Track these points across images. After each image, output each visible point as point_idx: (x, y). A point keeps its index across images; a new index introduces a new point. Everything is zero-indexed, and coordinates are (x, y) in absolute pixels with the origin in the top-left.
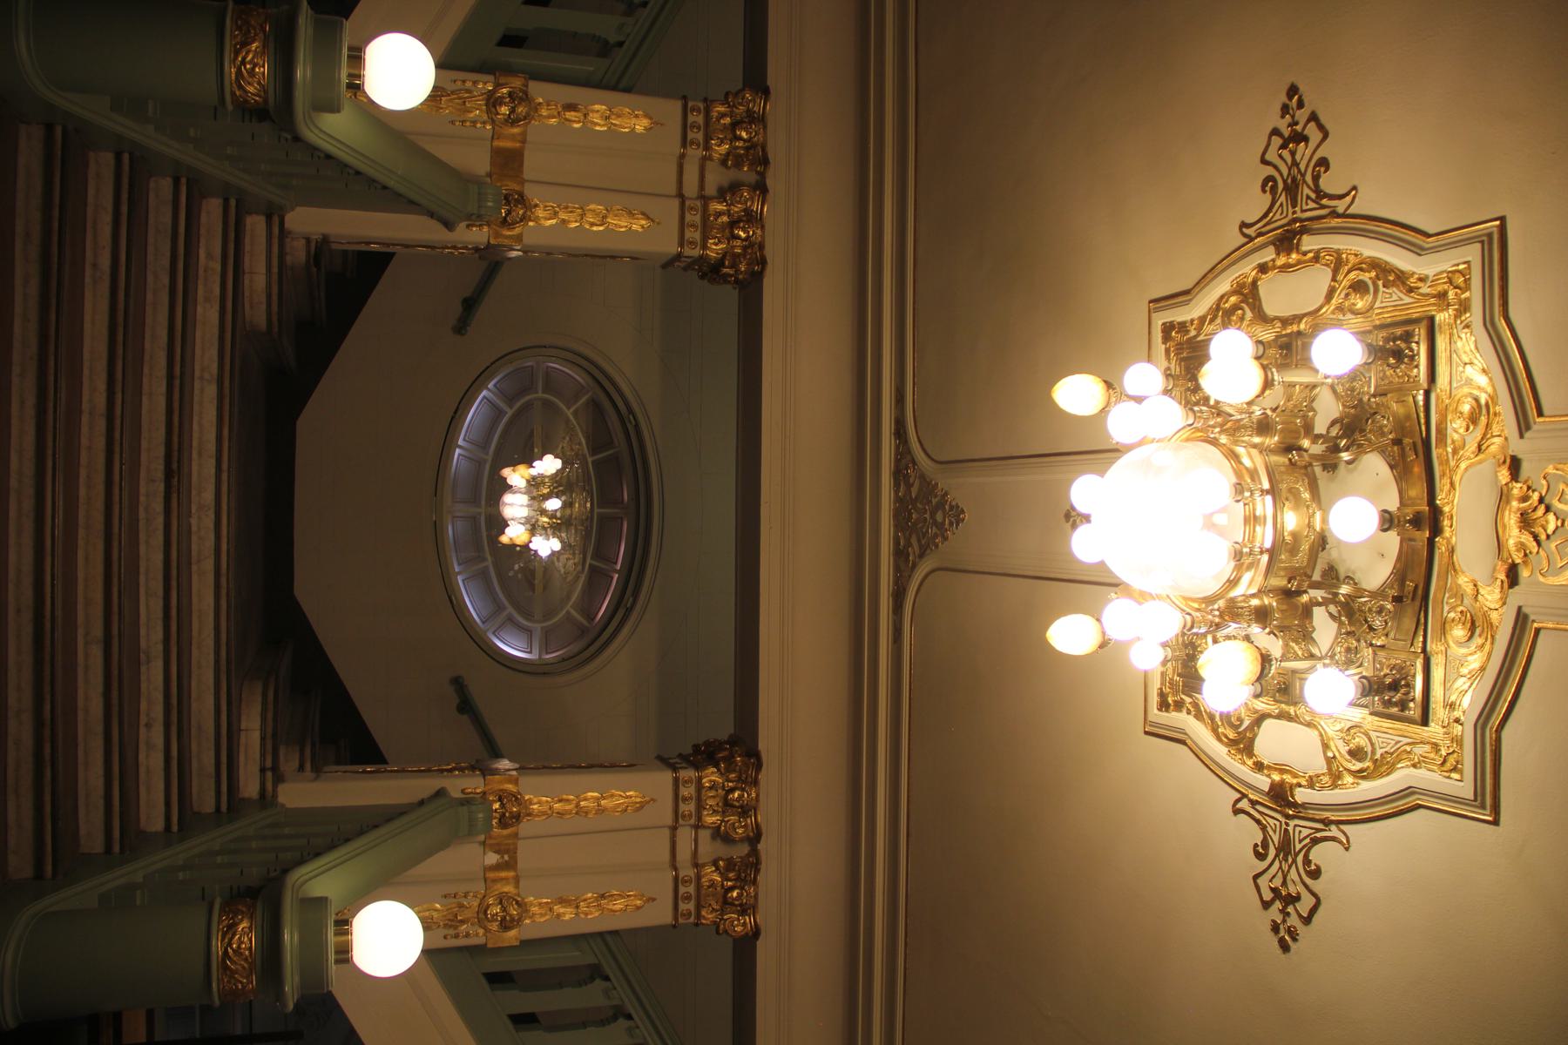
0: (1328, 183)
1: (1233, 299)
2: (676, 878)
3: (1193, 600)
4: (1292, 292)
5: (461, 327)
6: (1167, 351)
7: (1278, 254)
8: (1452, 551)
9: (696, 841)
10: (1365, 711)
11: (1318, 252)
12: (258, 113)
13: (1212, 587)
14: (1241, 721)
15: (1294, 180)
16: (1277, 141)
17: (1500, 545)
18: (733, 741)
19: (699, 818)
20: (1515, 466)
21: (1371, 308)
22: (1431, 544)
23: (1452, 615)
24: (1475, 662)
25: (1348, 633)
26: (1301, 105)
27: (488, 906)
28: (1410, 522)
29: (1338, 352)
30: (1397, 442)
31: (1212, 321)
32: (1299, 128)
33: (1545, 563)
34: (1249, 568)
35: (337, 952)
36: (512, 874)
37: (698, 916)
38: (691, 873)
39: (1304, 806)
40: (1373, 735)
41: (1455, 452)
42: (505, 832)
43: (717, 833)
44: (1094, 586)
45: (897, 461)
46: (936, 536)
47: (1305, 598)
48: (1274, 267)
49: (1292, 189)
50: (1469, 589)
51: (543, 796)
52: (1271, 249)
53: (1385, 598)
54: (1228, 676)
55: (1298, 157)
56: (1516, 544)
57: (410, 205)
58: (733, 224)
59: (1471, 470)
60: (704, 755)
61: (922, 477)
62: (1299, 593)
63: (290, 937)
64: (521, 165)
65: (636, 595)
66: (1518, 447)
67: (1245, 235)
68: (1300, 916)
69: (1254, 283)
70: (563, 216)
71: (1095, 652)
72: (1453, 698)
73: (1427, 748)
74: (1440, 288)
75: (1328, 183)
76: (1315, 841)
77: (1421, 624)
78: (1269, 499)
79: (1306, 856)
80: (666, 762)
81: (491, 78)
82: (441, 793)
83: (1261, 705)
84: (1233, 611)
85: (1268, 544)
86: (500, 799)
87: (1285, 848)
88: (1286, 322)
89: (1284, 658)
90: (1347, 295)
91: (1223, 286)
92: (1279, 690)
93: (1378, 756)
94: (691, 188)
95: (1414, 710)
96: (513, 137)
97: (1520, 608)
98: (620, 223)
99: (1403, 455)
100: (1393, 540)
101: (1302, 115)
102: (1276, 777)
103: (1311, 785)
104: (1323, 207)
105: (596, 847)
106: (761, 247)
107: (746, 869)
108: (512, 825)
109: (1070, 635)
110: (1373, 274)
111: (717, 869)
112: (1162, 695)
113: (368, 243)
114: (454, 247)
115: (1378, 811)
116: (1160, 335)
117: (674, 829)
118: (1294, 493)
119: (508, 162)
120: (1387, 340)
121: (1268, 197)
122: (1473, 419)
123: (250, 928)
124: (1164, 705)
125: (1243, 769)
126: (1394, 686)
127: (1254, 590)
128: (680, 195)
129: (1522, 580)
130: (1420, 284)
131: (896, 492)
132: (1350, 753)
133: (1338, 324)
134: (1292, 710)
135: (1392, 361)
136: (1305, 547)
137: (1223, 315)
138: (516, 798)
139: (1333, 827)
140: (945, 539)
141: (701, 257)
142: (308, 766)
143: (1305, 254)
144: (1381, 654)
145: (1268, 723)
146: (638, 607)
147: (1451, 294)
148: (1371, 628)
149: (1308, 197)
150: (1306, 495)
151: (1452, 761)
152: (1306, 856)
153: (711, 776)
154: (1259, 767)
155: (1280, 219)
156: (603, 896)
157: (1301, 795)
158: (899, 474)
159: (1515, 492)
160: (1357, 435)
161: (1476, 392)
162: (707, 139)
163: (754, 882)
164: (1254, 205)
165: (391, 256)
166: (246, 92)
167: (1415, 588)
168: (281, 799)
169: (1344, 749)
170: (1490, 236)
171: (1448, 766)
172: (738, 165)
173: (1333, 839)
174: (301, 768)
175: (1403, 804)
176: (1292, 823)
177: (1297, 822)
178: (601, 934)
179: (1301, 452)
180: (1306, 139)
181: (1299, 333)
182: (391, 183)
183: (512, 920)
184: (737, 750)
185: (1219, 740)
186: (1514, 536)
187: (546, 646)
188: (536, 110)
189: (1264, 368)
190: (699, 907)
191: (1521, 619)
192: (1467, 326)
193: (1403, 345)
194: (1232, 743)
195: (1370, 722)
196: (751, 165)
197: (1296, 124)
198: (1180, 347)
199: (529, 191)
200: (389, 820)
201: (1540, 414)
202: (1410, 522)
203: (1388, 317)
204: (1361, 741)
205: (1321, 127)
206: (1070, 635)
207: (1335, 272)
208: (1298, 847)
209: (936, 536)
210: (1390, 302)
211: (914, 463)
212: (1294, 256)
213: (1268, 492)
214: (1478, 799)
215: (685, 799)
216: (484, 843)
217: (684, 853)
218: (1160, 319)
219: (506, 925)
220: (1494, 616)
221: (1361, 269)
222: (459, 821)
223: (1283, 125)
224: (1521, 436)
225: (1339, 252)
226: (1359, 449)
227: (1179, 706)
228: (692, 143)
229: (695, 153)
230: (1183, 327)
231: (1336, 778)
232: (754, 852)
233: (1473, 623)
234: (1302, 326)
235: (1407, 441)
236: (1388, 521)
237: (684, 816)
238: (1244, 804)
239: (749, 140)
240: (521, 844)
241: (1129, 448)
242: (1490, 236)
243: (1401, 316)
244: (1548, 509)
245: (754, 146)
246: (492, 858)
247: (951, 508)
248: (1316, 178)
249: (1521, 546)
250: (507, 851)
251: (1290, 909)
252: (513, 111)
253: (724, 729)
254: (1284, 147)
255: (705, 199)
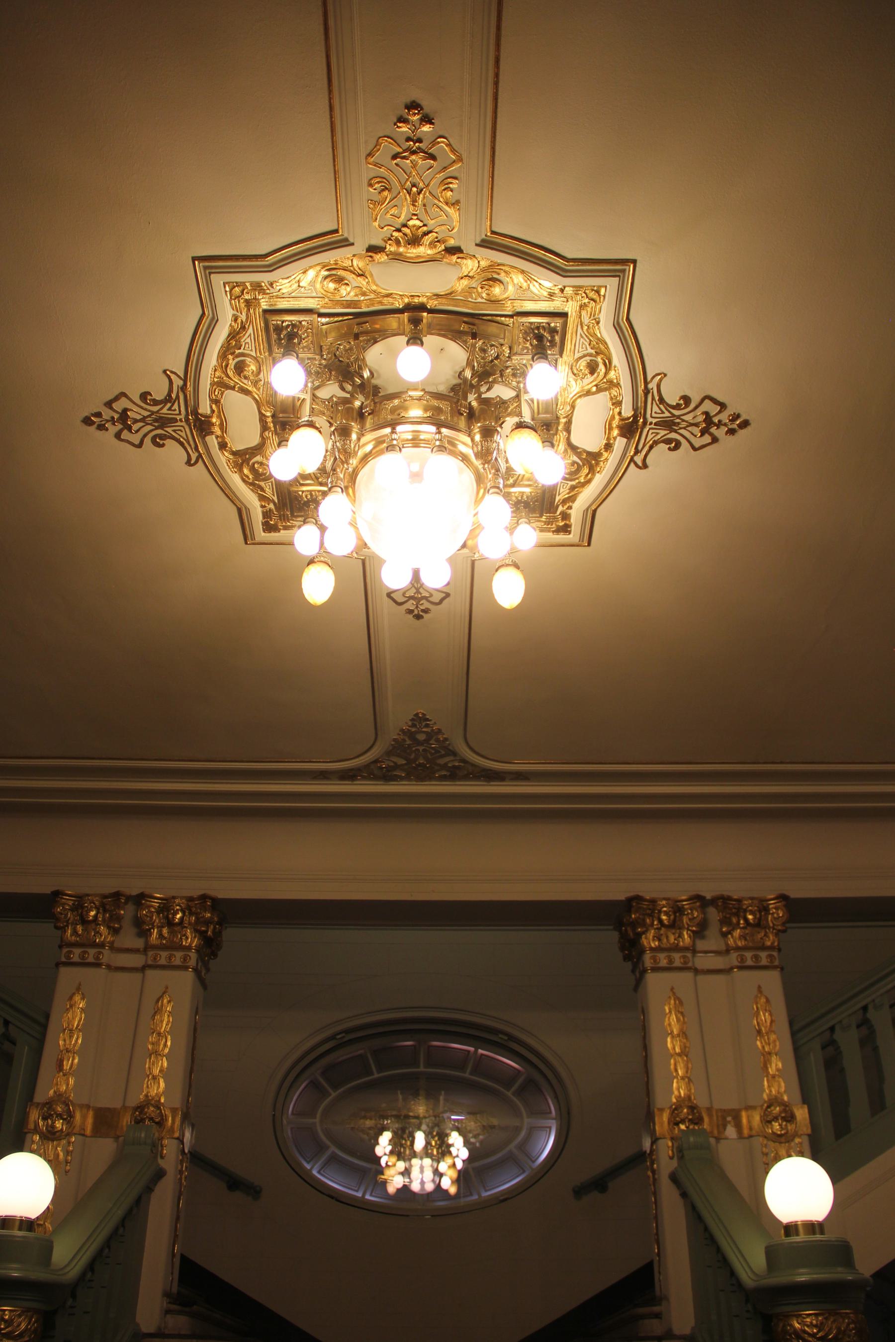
0: (159, 393)
1: (246, 471)
2: (741, 968)
3: (478, 493)
4: (242, 422)
5: (254, 1191)
6: (286, 528)
7: (212, 433)
8: (437, 296)
9: (706, 952)
10: (560, 360)
11: (211, 400)
12: (47, 1321)
13: (469, 477)
14: (574, 463)
15: (156, 420)
16: (125, 435)
17: (432, 260)
18: (619, 925)
19: (686, 949)
20: (373, 249)
21: (256, 359)
22: (431, 311)
23: (484, 295)
24: (519, 279)
25: (502, 376)
26: (98, 415)
27: (774, 1133)
28: (416, 326)
29: (288, 377)
30: (356, 337)
31: (262, 490)
32: (116, 416)
33: (443, 228)
34: (454, 445)
35: (814, 1233)
36: (744, 1114)
37: (771, 948)
38: (734, 955)
39: (635, 409)
40: (577, 355)
41: (364, 294)
42: (706, 1119)
43: (700, 932)
44: (472, 572)
45: (376, 778)
46: (437, 740)
47: (474, 404)
48: (223, 437)
49: (163, 422)
50: (465, 282)
51: (675, 1087)
52: (208, 438)
53: (474, 346)
54: (537, 461)
55: (139, 417)
56: (431, 248)
57: (138, 1207)
58: (170, 924)
59: (378, 282)
60: (631, 948)
61: (389, 753)
62: (471, 408)
63: (803, 1276)
64: (109, 1109)
65: (496, 1031)
66: (360, 247)
67: (196, 462)
68: (720, 412)
69: (234, 453)
70: (156, 1071)
71: (522, 571)
72: (545, 294)
73: (584, 313)
74: (243, 305)
75: (159, 393)
76: (662, 400)
77: (492, 319)
78: (399, 428)
79: (674, 407)
80: (639, 982)
81: (29, 1136)
82: (674, 1178)
83: (562, 447)
84: (485, 455)
85: (433, 429)
86: (677, 1124)
87: (668, 424)
88: (264, 428)
89: (520, 414)
90: (246, 378)
91: (235, 479)
92: (548, 430)
93: (593, 351)
94: (136, 960)
95: (556, 323)
96: (84, 1117)
97: (477, 245)
98: (165, 1023)
99: (366, 333)
100: (430, 340)
101: (107, 414)
102: (616, 432)
103: (618, 404)
104: (178, 397)
105: (710, 1036)
106: (190, 899)
107: (729, 907)
108: (700, 1113)
109: (509, 590)
110: (230, 357)
111: (729, 932)
112: (558, 530)
113: (173, 1255)
114: (181, 1172)
115: (635, 351)
116: (273, 534)
117: (697, 971)
118: (394, 410)
119: (105, 1120)
120: (280, 345)
121: (168, 442)
122: (340, 280)
123: (798, 1316)
124: (566, 529)
125: (611, 460)
126: (540, 338)
127: (468, 440)
128: (143, 969)
129: (457, 244)
130: (239, 321)
131: (402, 779)
132: (592, 373)
133: (268, 384)
134: (563, 420)
135: (296, 341)
136: (435, 403)
137: (258, 478)
138: (675, 1110)
139: (650, 386)
140: (439, 731)
141: (197, 951)
142: (656, 1309)
143: (213, 411)
144: (515, 349)
145: (574, 440)
146: (509, 1030)
147: (247, 297)
148: (497, 358)
149: (169, 409)
150: (396, 402)
151: (592, 295)
152: (674, 407)
153: (649, 940)
154: (608, 447)
155: (185, 432)
156: (759, 1032)
157: (627, 412)
158: (387, 776)
159: (392, 249)
160: (352, 369)
161: (320, 279)
162: (94, 945)
163: (739, 901)
164: (173, 453)
165: (184, 1260)
166: (26, 1330)
167: (466, 323)
168: (687, 1331)
169: (590, 378)
170: (205, 268)
171: (595, 297)
172: (119, 919)
173: (658, 386)
174: (658, 1316)
175: (626, 331)
176: (650, 420)
177: (648, 416)
178: (793, 1034)
179: (361, 406)
180: (125, 410)
181: (273, 416)
182: (120, 1213)
183: (785, 1111)
184: (623, 920)
185: (589, 482)
186: (423, 251)
187: (546, 1114)
188: (60, 1095)
189: (299, 427)
190: (763, 948)
191: (484, 244)
192: (271, 284)
193: (285, 332)
194: (592, 470)
195: (567, 357)
196: (119, 908)
197: (113, 418)
198: (283, 518)
199: (132, 1102)
200: (700, 1218)
201: (336, 231)
202: (416, 326)
203: (263, 346)
204: (583, 364)
205: (116, 399)
206: (509, 590)
207: (228, 387)
208: (667, 414)
209: (437, 740)
210: (249, 342)
211: (376, 761)
212: (214, 420)
213: (394, 429)
214: (619, 274)
215: (671, 961)
216: (718, 1139)
217: (718, 962)
218: (261, 535)
219: (790, 1117)
220: (484, 264)
221: (227, 366)
222: (696, 1154)
223: (113, 429)
224: (353, 244)
225: (212, 384)
226: (361, 364)
227: (565, 516)
228: (98, 958)
229: (106, 956)
230: (267, 515)
231: (612, 385)
232: (713, 901)
233: (489, 280)
234: (268, 414)
235: (356, 330)
236: (415, 339)
237: (685, 963)
238: (639, 459)
239: (97, 909)
240: (716, 1106)
241: (360, 538)
242: (205, 268)
243: (262, 335)
244: (405, 226)
245: (103, 905)
246: (731, 1131)
247: (414, 726)
248: (156, 402)
249: (432, 245)
250: (724, 1118)
251: (716, 420)
252: (60, 1116)
253: (610, 937)
254: (129, 429)
255: (147, 948)
